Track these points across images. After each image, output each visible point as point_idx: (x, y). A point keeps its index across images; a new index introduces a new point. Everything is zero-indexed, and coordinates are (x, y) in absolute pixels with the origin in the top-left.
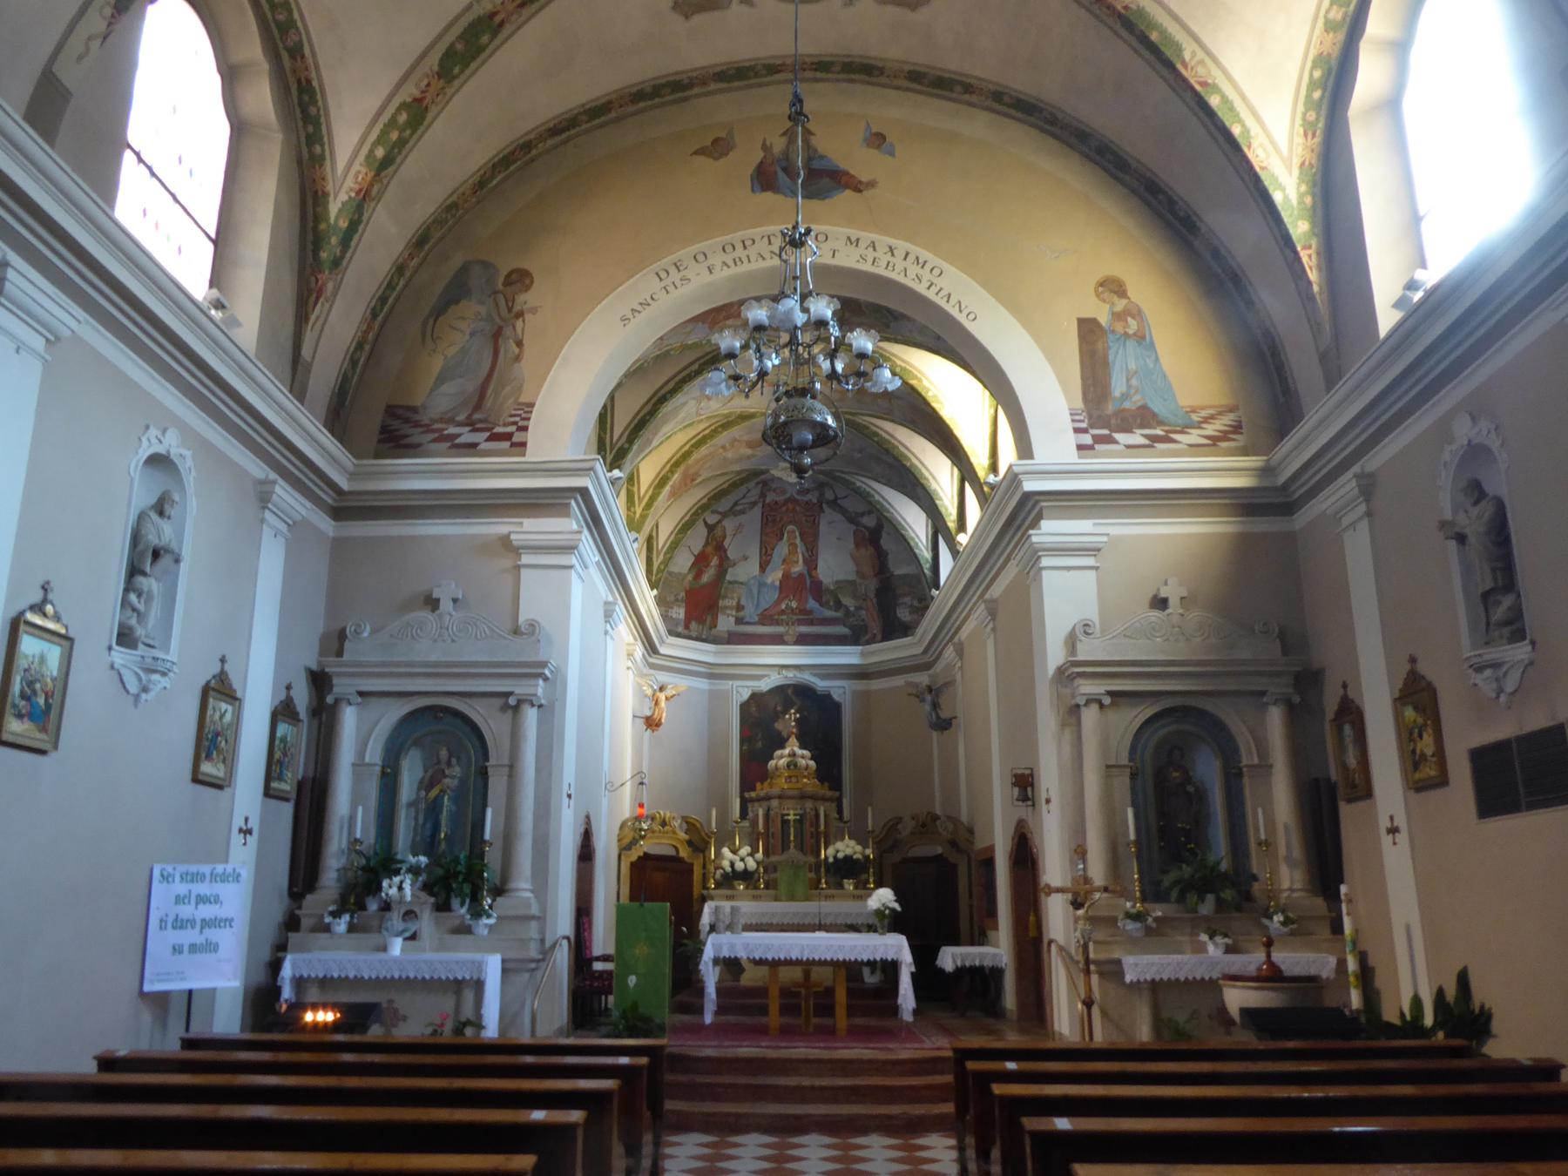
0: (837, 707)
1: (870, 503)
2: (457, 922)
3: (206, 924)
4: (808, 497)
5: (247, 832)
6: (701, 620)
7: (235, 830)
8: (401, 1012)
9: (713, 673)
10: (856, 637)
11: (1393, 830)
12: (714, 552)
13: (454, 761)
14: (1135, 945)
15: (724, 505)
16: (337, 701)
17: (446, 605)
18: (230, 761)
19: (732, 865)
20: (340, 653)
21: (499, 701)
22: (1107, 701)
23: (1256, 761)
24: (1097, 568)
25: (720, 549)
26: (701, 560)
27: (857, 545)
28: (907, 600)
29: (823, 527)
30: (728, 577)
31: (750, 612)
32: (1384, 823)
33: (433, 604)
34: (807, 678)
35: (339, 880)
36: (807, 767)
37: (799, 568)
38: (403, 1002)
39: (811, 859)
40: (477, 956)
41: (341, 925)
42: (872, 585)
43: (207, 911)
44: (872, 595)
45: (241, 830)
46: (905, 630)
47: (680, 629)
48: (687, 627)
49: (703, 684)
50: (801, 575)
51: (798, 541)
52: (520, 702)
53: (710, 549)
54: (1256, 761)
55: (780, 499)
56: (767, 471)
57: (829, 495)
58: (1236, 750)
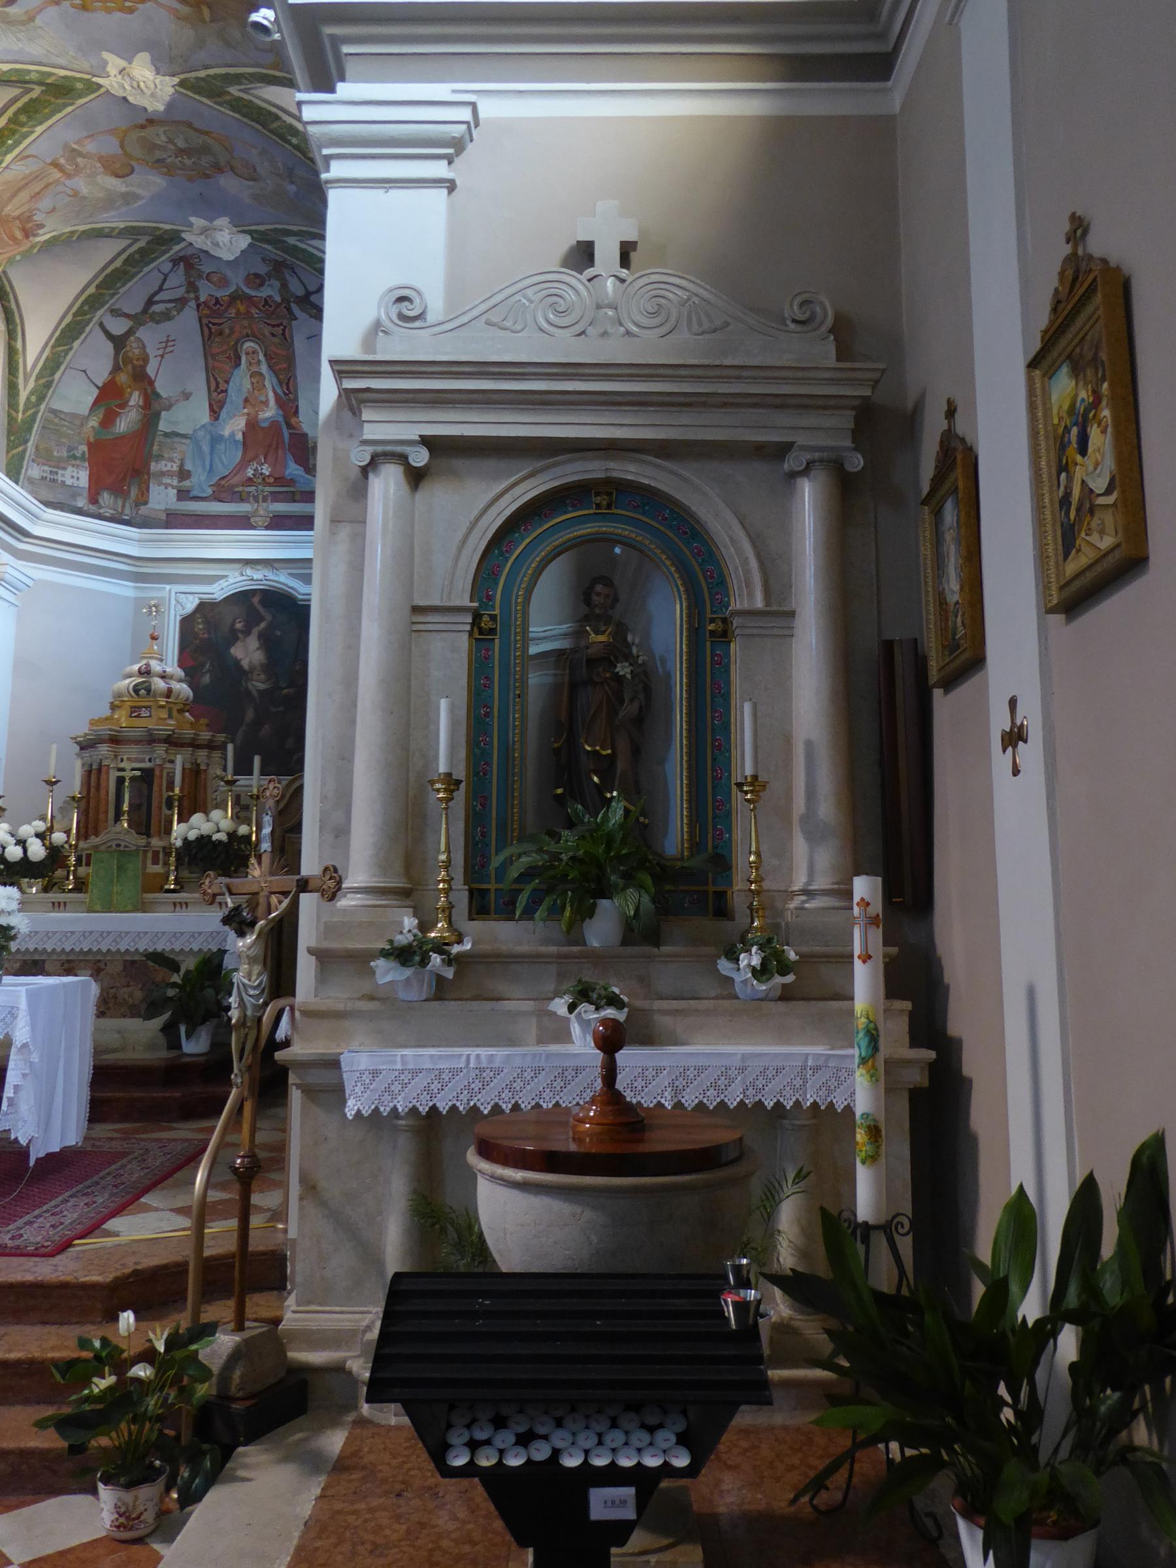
4: (264, 292)
6: (118, 491)
9: (142, 572)
11: (1014, 737)
12: (130, 378)
14: (390, 1018)
15: (132, 297)
22: (420, 457)
23: (759, 603)
24: (451, 186)
25: (141, 378)
26: (109, 397)
30: (163, 426)
31: (200, 481)
32: (1000, 722)
36: (169, 693)
37: (270, 412)
47: (81, 503)
48: (94, 500)
49: (126, 589)
50: (274, 424)
51: (264, 368)
53: (123, 378)
54: (759, 603)
55: (223, 294)
56: (175, 237)
58: (720, 583)
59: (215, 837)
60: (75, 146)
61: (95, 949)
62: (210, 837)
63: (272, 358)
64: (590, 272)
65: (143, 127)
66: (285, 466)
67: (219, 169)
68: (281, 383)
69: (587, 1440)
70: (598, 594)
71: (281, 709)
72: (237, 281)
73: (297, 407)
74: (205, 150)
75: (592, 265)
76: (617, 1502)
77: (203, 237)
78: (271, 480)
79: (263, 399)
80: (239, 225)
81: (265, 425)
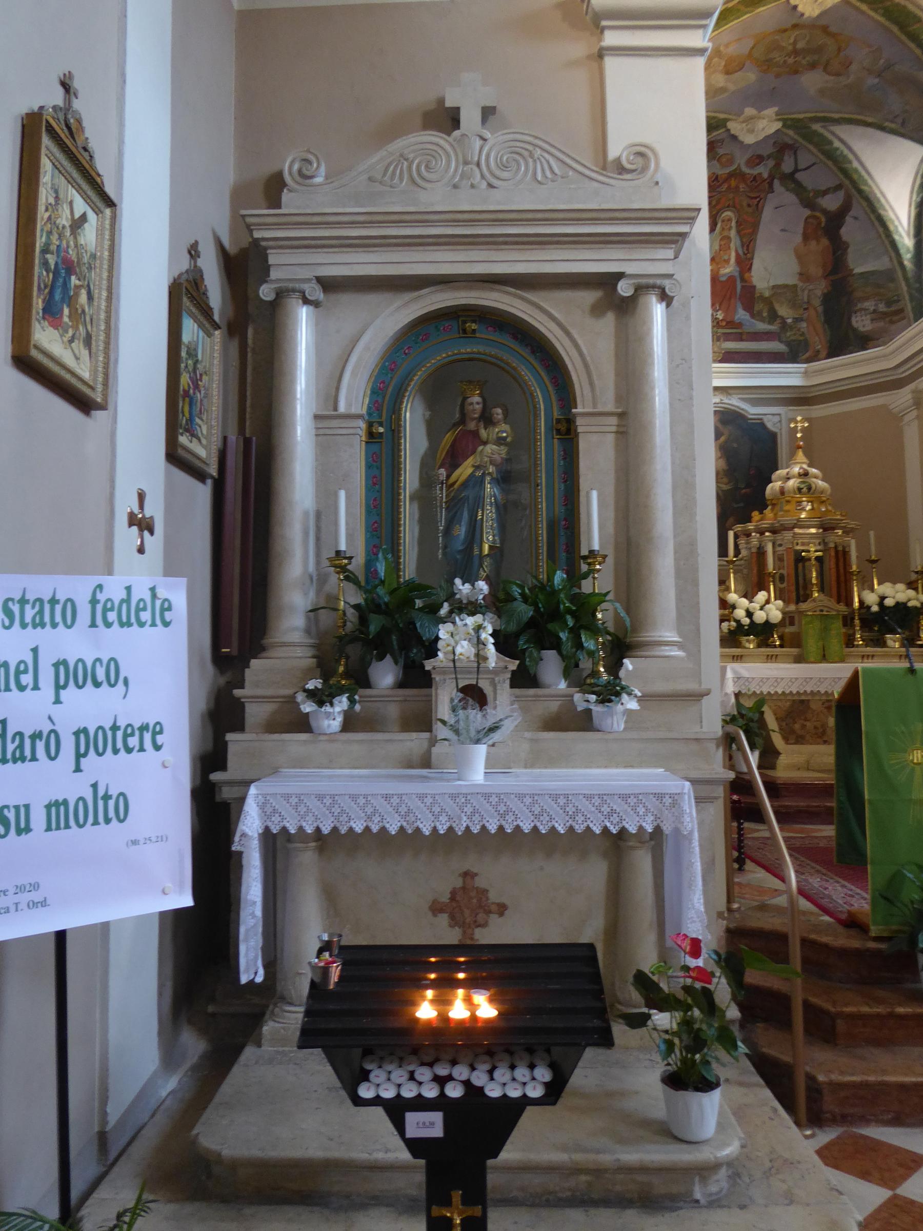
0: (773, 437)
1: (846, 173)
2: (554, 706)
3: (88, 742)
5: (144, 525)
7: (121, 519)
8: (493, 897)
10: (794, 353)
13: (498, 412)
16: (281, 294)
17: (470, 118)
18: (102, 340)
19: (749, 614)
20: (274, 201)
21: (590, 297)
27: (806, 237)
28: (869, 305)
29: (767, 213)
33: (447, 119)
34: (735, 402)
35: (308, 631)
38: (494, 875)
39: (842, 608)
40: (835, 822)
41: (332, 717)
42: (820, 288)
43: (87, 707)
44: (817, 302)
45: (133, 520)
46: (864, 341)
50: (731, 279)
51: (733, 233)
52: (641, 289)
57: (787, 166)
59: (910, 604)
60: (722, 48)
61: (787, 692)
62: (905, 604)
63: (741, 225)
64: (456, 133)
65: (785, 31)
66: (735, 311)
67: (813, 66)
68: (743, 246)
69: (399, 1075)
70: (478, 403)
71: (742, 505)
72: (741, 161)
73: (751, 264)
74: (819, 50)
75: (459, 128)
76: (428, 1124)
77: (744, 125)
78: (724, 324)
79: (726, 257)
80: (779, 116)
81: (724, 279)
